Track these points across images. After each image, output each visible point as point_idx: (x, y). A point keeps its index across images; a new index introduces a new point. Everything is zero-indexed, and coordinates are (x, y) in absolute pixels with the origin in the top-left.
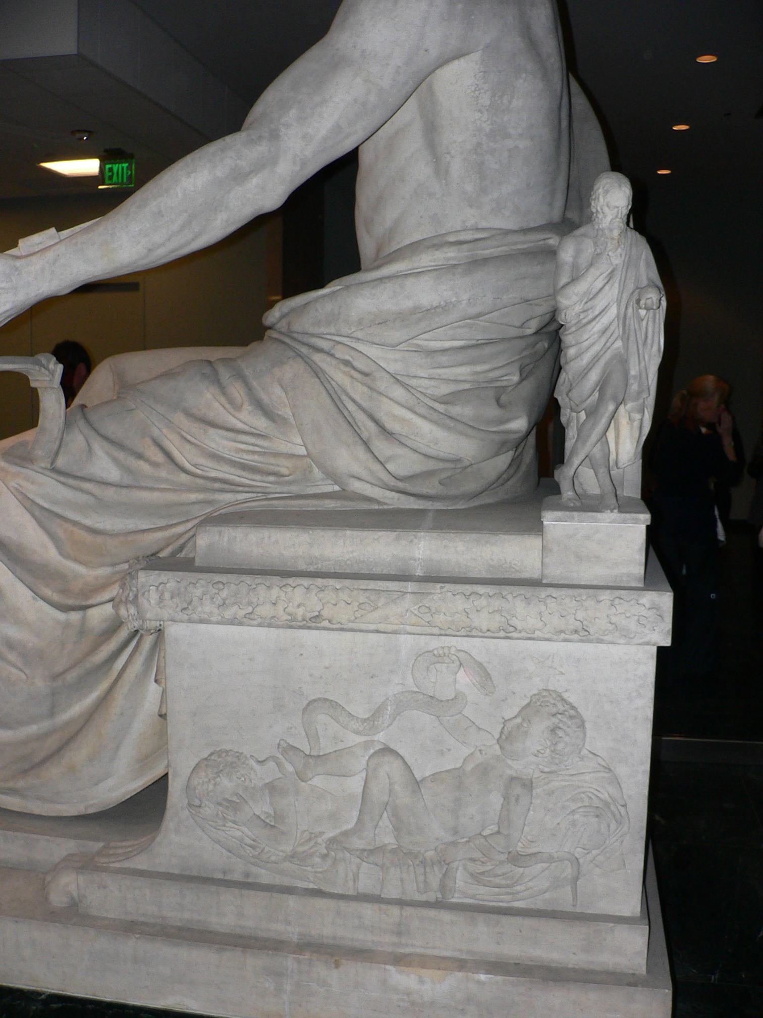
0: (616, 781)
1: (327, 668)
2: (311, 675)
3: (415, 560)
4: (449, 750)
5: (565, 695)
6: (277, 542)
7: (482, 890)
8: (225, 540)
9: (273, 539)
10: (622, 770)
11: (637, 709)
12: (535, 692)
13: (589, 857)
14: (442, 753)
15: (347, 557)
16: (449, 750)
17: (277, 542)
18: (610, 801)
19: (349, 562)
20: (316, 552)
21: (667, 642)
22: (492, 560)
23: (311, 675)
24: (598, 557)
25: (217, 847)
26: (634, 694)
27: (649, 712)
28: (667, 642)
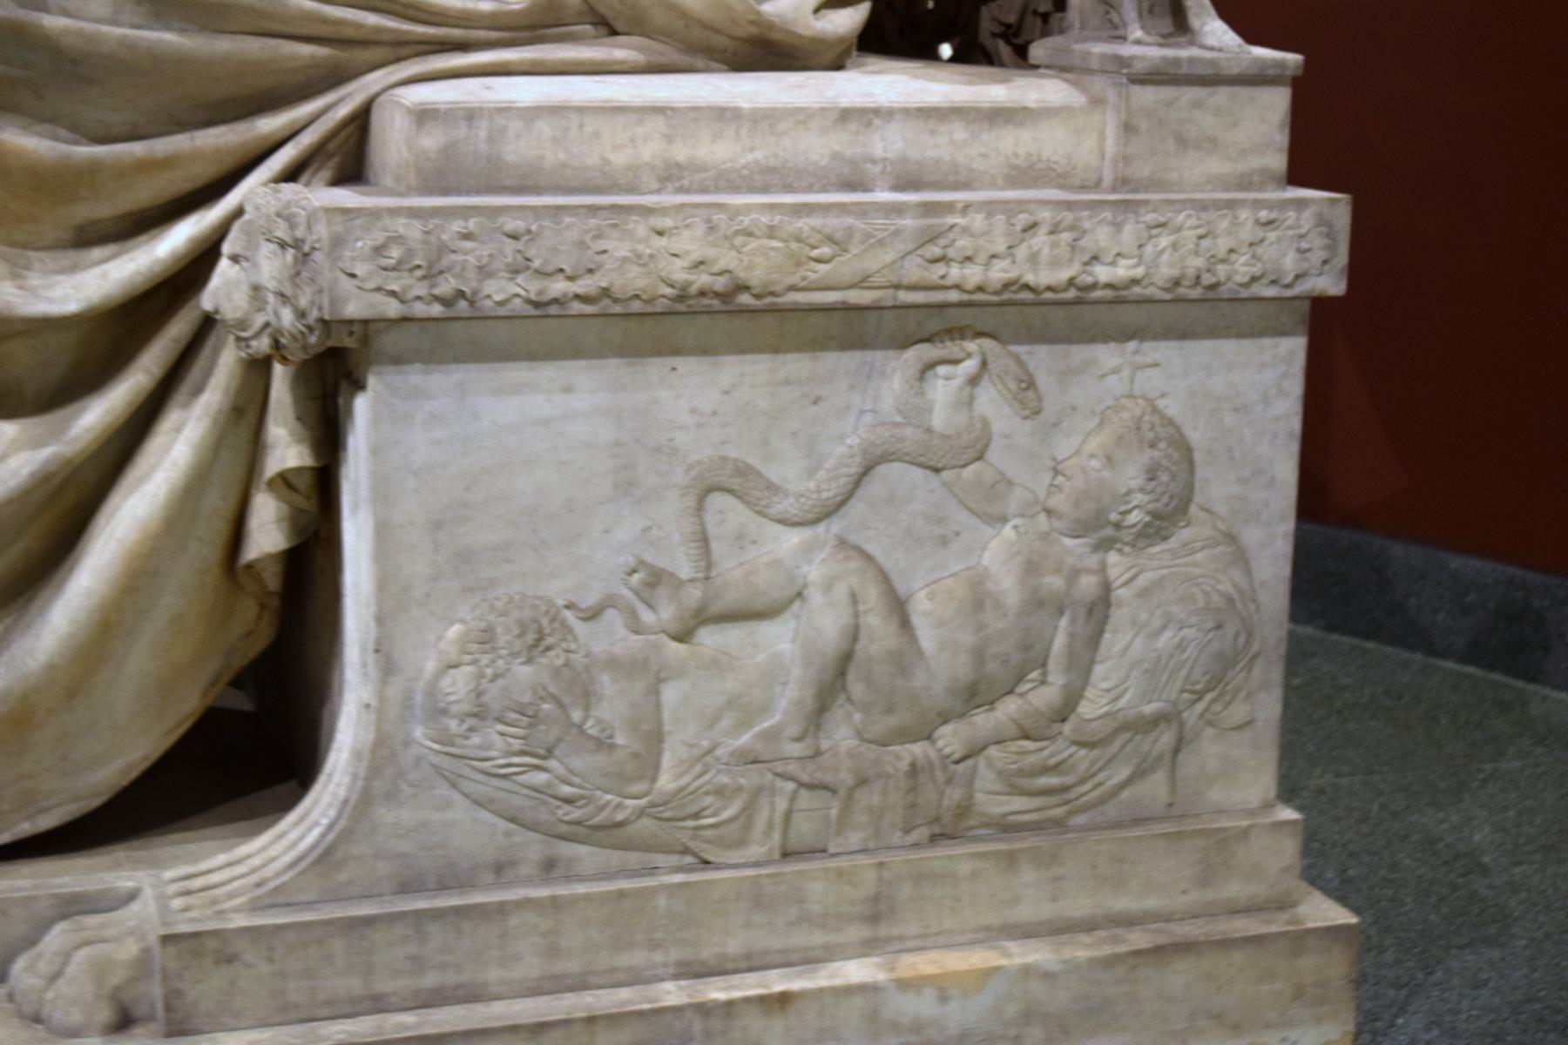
0: (1241, 558)
1: (726, 393)
2: (693, 411)
3: (874, 162)
4: (957, 534)
5: (1161, 403)
6: (597, 135)
7: (1019, 803)
8: (483, 134)
9: (589, 129)
10: (1251, 536)
11: (1277, 419)
12: (1109, 402)
13: (1200, 707)
14: (944, 542)
15: (742, 161)
16: (957, 534)
17: (597, 135)
18: (1236, 596)
19: (745, 172)
20: (830, 94)
21: (1332, 284)
22: (1016, 155)
23: (693, 411)
24: (1213, 141)
25: (485, 815)
26: (1273, 391)
27: (1296, 424)
28: (1332, 284)
